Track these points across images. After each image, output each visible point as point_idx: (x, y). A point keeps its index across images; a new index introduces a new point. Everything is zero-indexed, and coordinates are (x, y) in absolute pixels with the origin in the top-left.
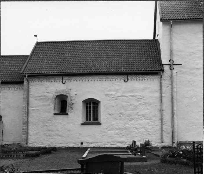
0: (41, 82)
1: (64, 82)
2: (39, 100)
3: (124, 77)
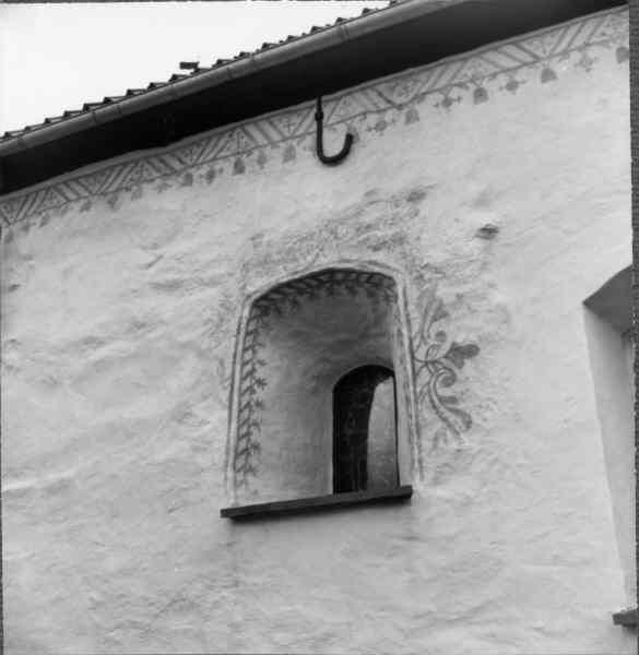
0: (112, 203)
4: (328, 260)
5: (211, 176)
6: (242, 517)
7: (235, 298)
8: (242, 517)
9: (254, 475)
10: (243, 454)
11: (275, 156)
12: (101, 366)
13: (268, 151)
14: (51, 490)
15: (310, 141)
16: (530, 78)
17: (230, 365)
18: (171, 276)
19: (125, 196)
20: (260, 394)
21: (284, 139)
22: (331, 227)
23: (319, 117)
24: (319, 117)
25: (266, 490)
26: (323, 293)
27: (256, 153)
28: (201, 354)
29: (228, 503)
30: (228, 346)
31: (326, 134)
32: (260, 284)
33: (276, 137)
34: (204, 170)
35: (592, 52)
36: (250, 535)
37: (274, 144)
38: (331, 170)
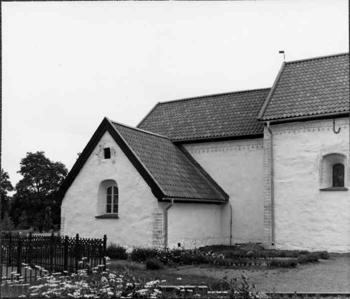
0: (294, 132)
1: (337, 130)
2: (292, 165)
3: (330, 123)
4: (335, 152)
5: (314, 130)
6: (322, 190)
7: (320, 156)
8: (322, 190)
9: (163, 269)
10: (321, 180)
11: (326, 129)
12: (295, 163)
13: (325, 128)
14: (288, 183)
15: (333, 127)
16: (292, 133)
17: (27, 274)
18: (308, 149)
19: (297, 131)
20: (323, 170)
21: (328, 126)
22: (336, 146)
23: (334, 123)
24: (334, 123)
25: (325, 186)
26: (91, 240)
27: (322, 128)
28: (315, 164)
29: (319, 188)
30: (319, 163)
31: (335, 127)
32: (324, 154)
33: (326, 125)
34: (312, 129)
35: (315, 129)
36: (323, 193)
37: (326, 127)
38: (338, 134)
